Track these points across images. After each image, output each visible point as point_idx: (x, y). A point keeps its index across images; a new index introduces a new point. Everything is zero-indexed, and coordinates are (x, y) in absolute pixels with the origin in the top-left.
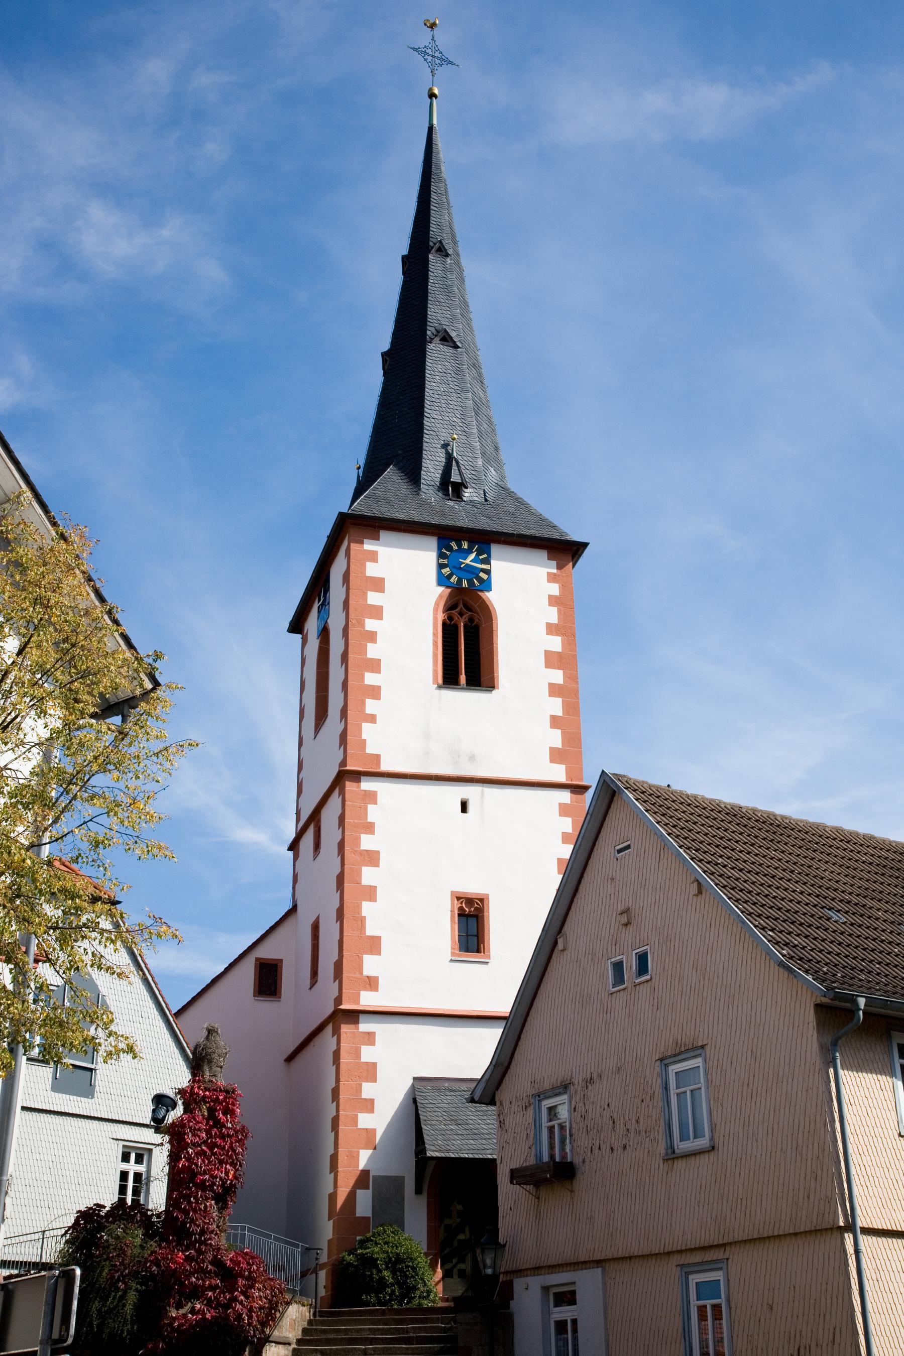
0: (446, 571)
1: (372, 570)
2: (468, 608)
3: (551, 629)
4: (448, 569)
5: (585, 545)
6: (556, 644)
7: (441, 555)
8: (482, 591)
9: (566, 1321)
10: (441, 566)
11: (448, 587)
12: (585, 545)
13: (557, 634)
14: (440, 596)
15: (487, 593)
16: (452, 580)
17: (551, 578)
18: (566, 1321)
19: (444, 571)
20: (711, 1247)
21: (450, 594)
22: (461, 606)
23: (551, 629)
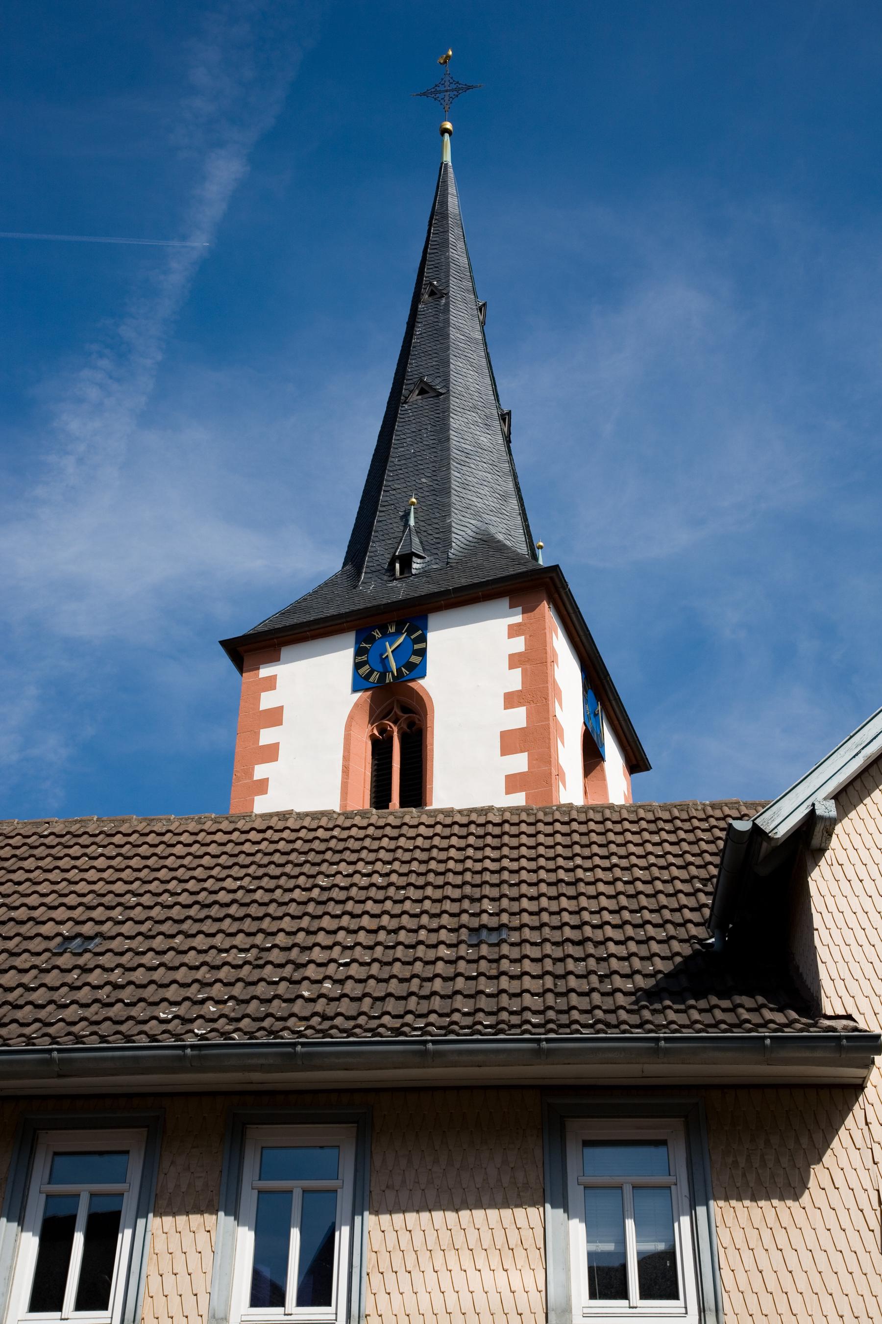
0: (365, 670)
1: (267, 701)
2: (406, 709)
3: (511, 700)
4: (367, 667)
5: (222, 643)
6: (518, 718)
7: (358, 653)
8: (413, 680)
9: (645, 1294)
10: (357, 666)
11: (366, 690)
12: (222, 643)
13: (520, 704)
14: (356, 705)
15: (421, 682)
16: (371, 680)
17: (514, 631)
18: (645, 1294)
19: (361, 671)
20: (101, 1153)
21: (373, 698)
22: (397, 710)
23: (511, 700)
